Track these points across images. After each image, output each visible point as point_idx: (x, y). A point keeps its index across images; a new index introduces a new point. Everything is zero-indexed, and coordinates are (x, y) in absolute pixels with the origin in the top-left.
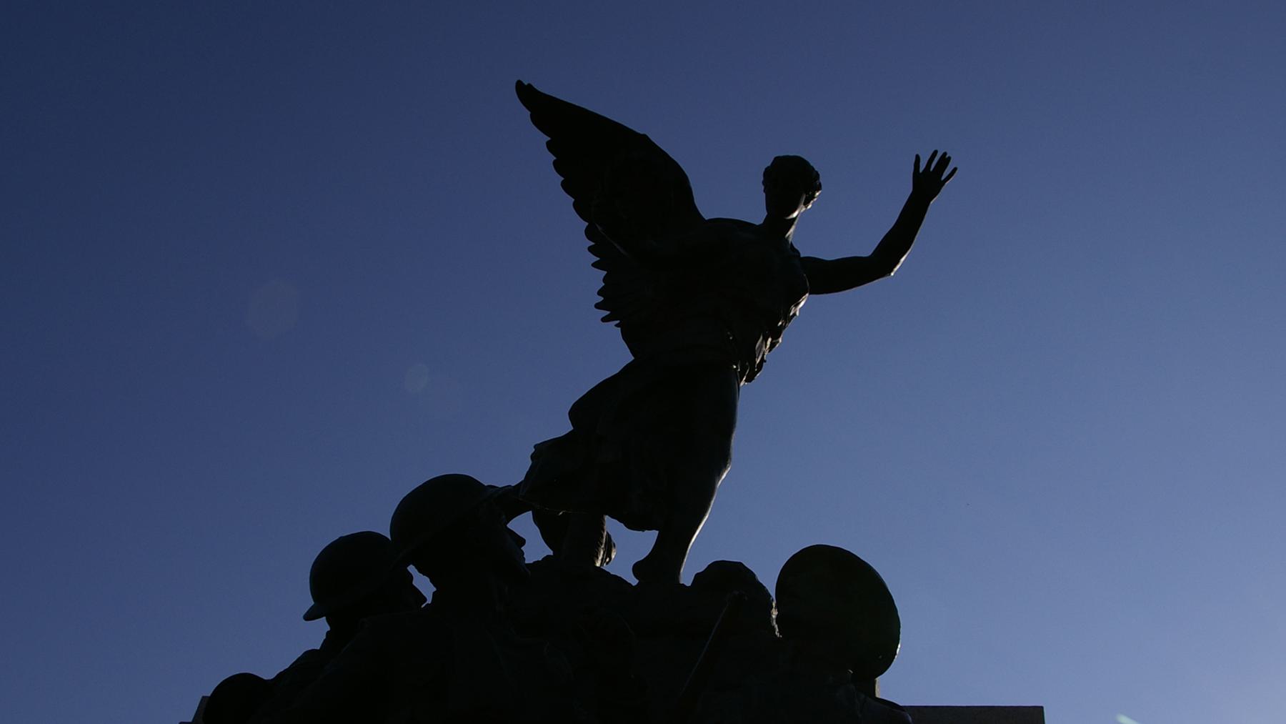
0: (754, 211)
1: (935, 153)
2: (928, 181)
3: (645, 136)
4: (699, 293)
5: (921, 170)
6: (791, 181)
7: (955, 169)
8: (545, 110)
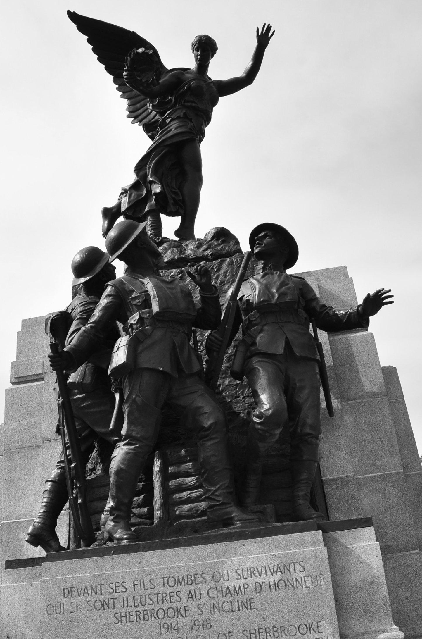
0: (190, 62)
1: (265, 24)
2: (264, 38)
3: (133, 32)
4: (173, 102)
5: (260, 34)
6: (205, 48)
7: (274, 32)
8: (83, 23)
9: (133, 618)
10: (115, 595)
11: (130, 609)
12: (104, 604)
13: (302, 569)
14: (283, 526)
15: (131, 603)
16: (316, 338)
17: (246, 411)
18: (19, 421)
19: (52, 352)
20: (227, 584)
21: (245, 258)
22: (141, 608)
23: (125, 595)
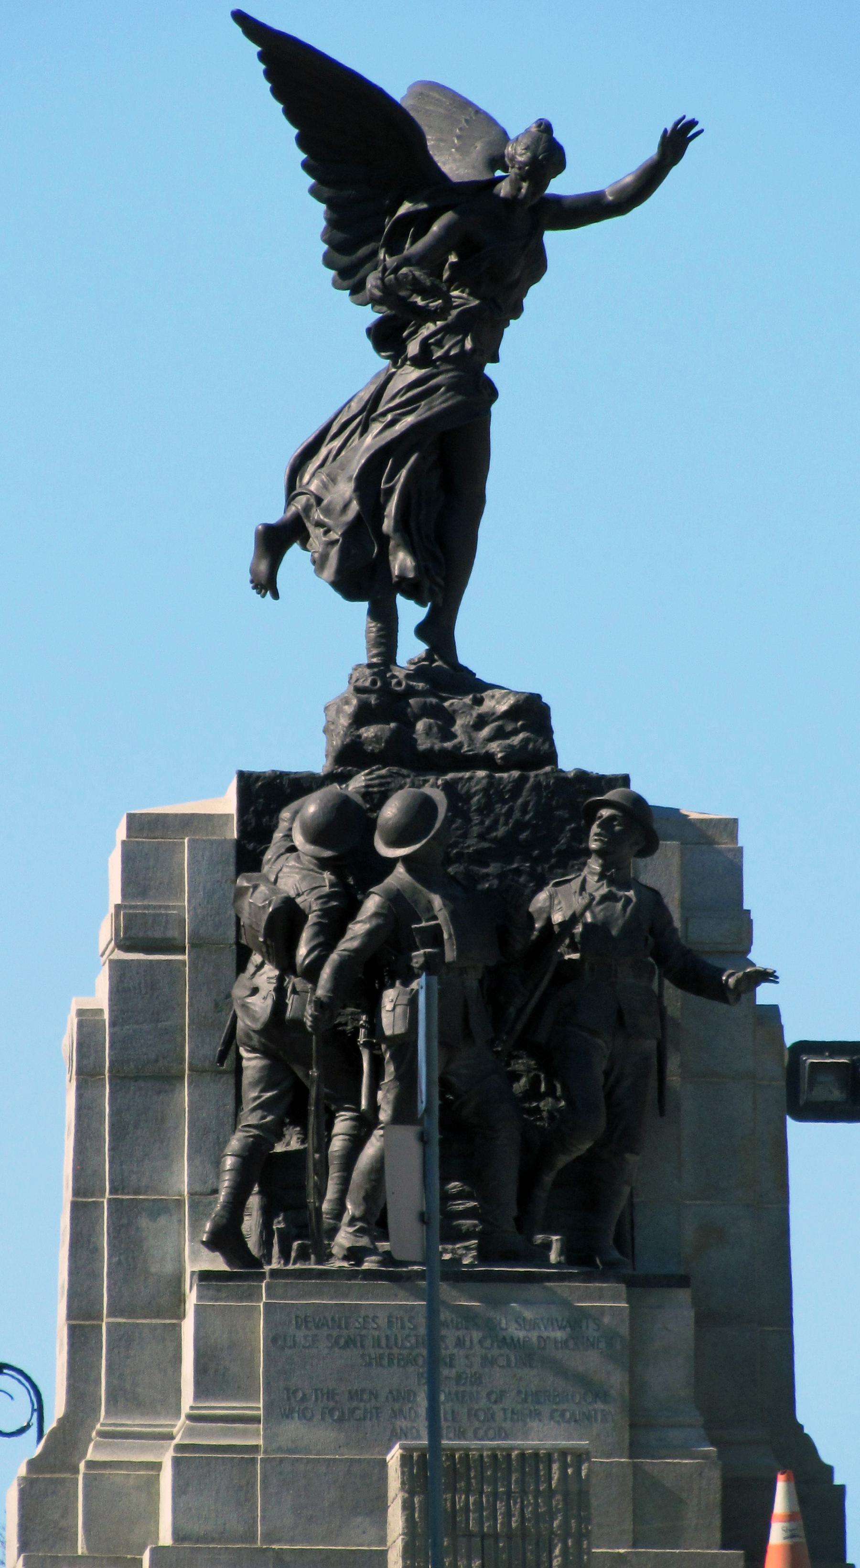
1: (684, 117)
2: (676, 141)
7: (701, 131)
8: (301, 77)
9: (385, 1362)
10: (364, 1332)
11: (381, 1351)
12: (350, 1342)
13: (596, 1328)
14: (96, 1251)
15: (383, 1343)
16: (660, 997)
17: (532, 1074)
18: (137, 1023)
19: (316, 1010)
20: (504, 1333)
21: (632, 905)
22: (395, 1351)
23: (376, 1333)
